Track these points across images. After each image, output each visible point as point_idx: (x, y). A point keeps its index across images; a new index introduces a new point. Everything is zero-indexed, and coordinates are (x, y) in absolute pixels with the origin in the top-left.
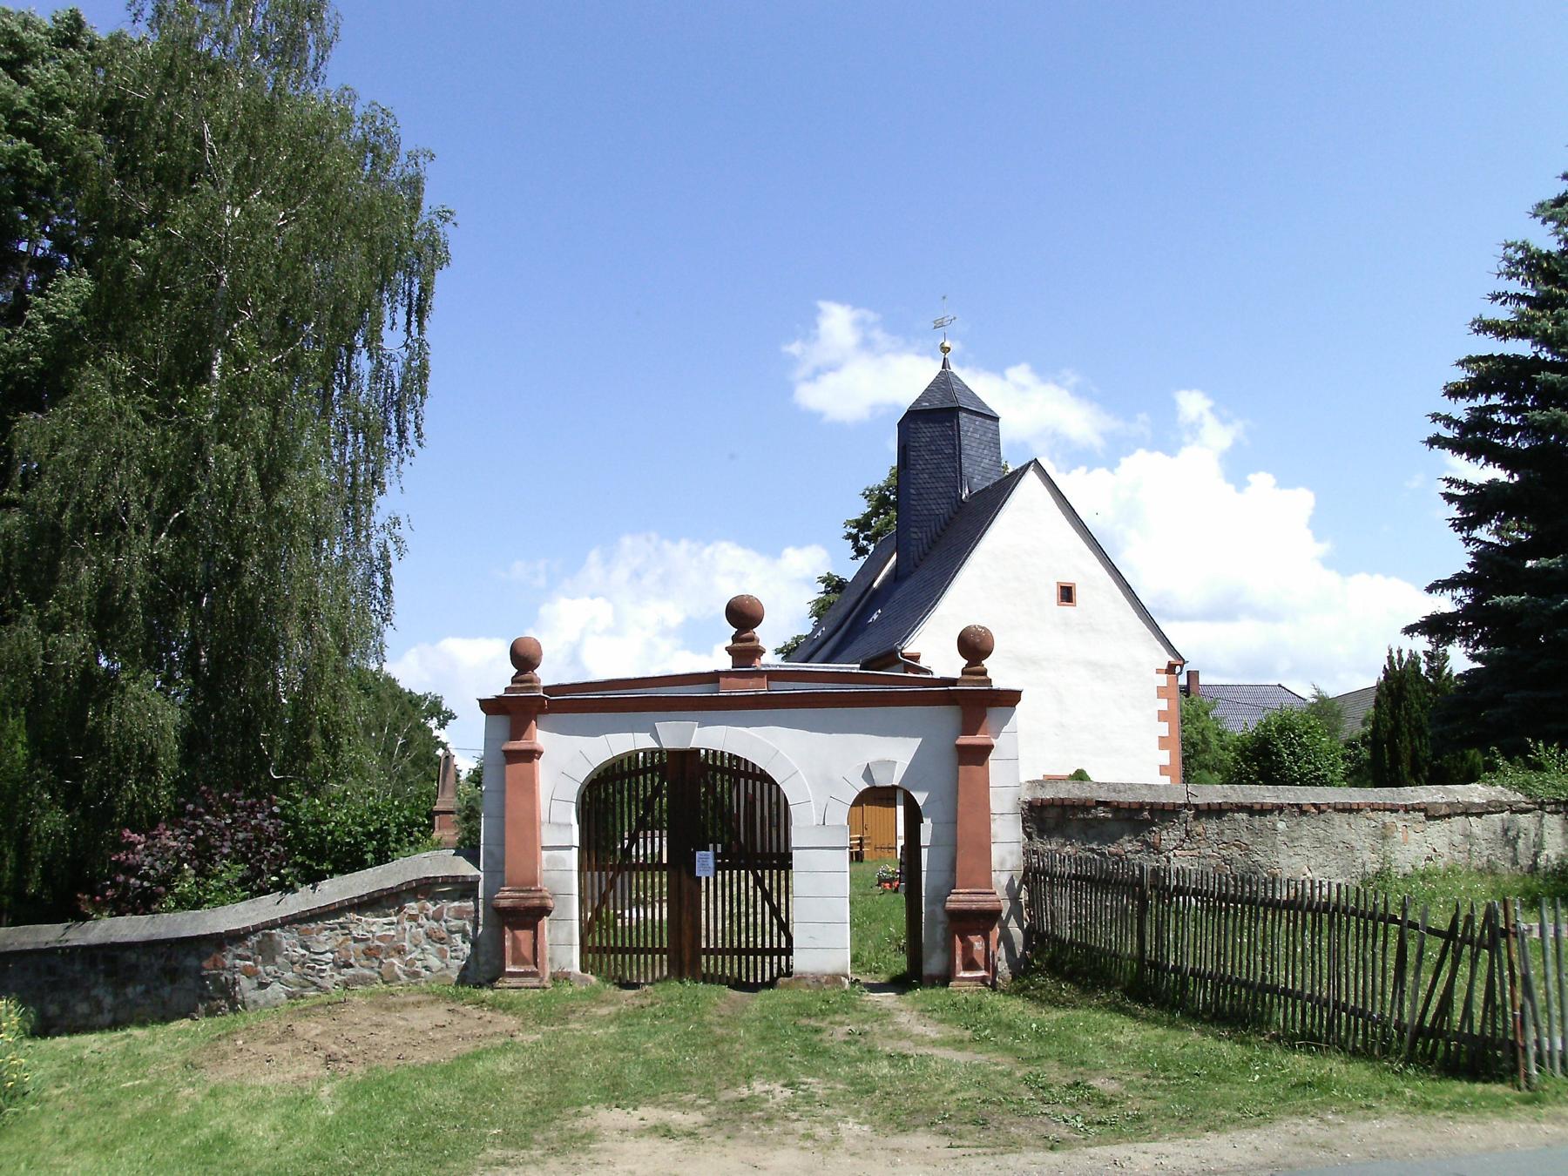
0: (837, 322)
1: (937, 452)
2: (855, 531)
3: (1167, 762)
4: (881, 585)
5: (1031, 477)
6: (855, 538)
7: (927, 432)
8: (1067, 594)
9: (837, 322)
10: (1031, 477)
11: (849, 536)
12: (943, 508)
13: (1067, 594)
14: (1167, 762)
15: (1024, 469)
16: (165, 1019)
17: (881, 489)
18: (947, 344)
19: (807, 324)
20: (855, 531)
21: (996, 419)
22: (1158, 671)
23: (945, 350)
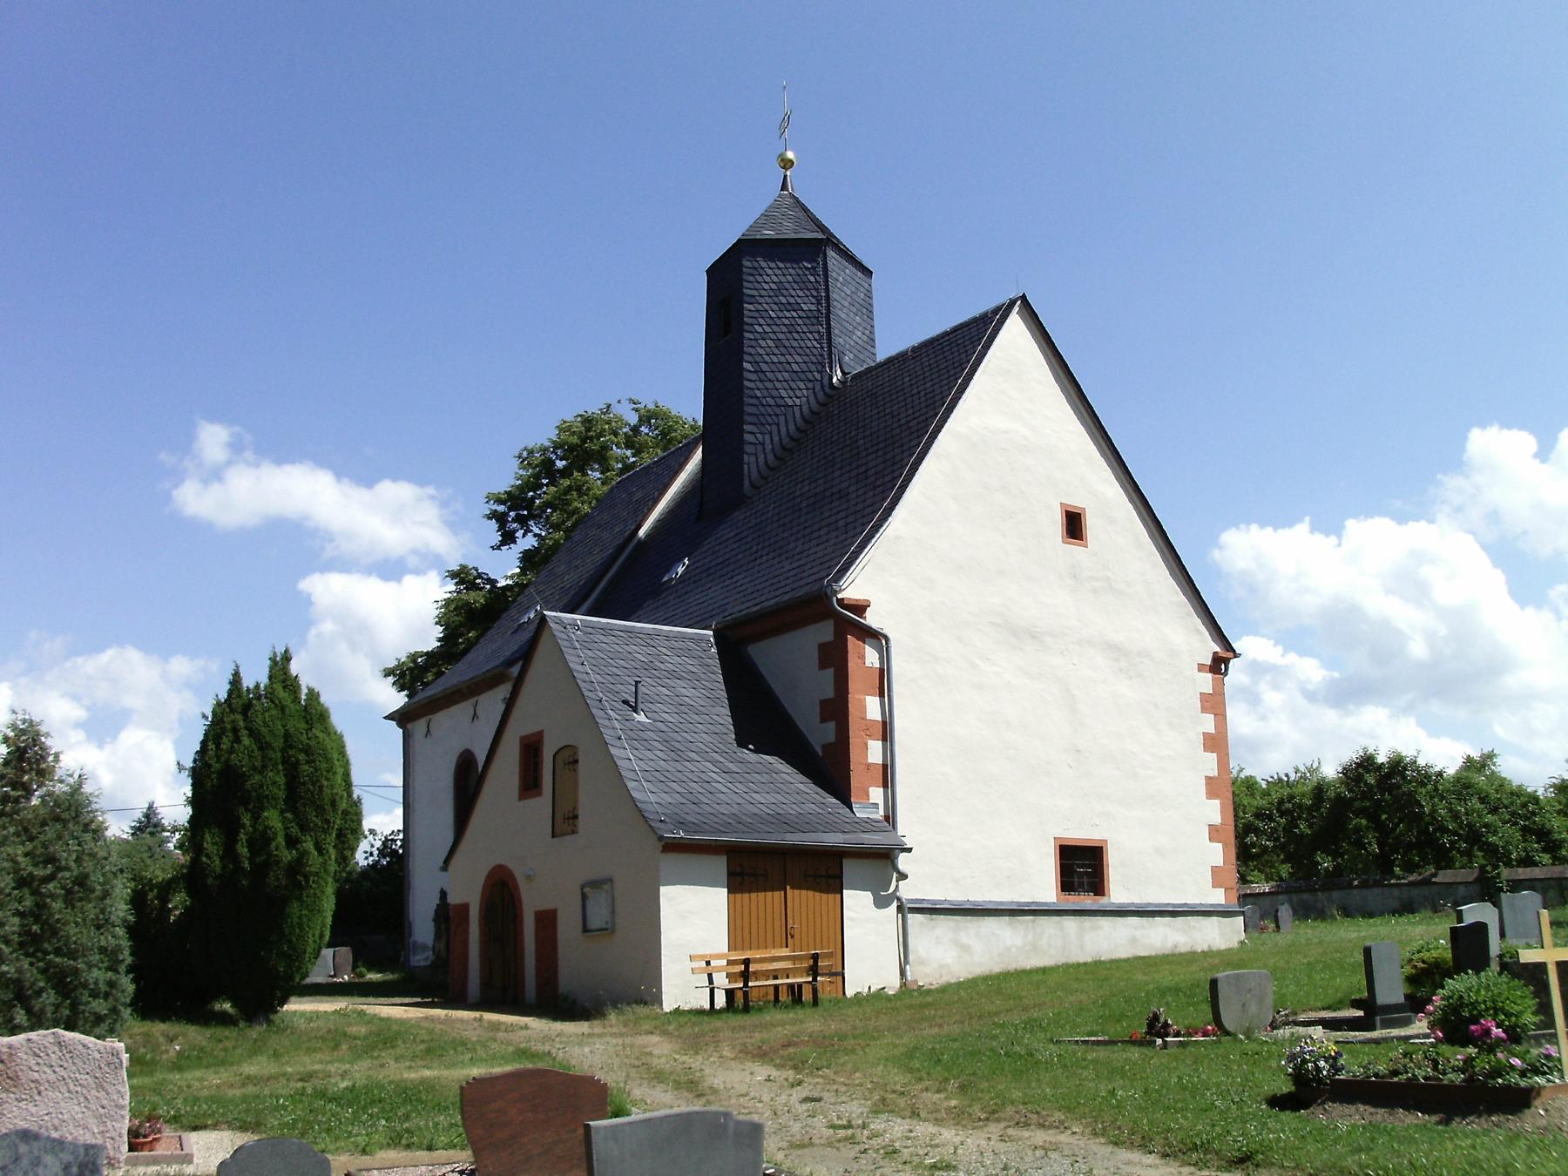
0: (213, 439)
1: (790, 307)
2: (501, 508)
3: (1217, 819)
4: (649, 535)
5: (1015, 326)
6: (500, 518)
7: (768, 276)
8: (1074, 525)
9: (213, 439)
10: (1015, 326)
11: (494, 515)
12: (799, 397)
13: (1074, 525)
14: (1217, 819)
15: (1012, 303)
16: (1097, 964)
17: (544, 450)
18: (790, 155)
19: (185, 443)
20: (501, 508)
21: (868, 273)
22: (1201, 667)
23: (787, 164)
